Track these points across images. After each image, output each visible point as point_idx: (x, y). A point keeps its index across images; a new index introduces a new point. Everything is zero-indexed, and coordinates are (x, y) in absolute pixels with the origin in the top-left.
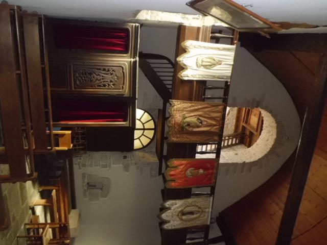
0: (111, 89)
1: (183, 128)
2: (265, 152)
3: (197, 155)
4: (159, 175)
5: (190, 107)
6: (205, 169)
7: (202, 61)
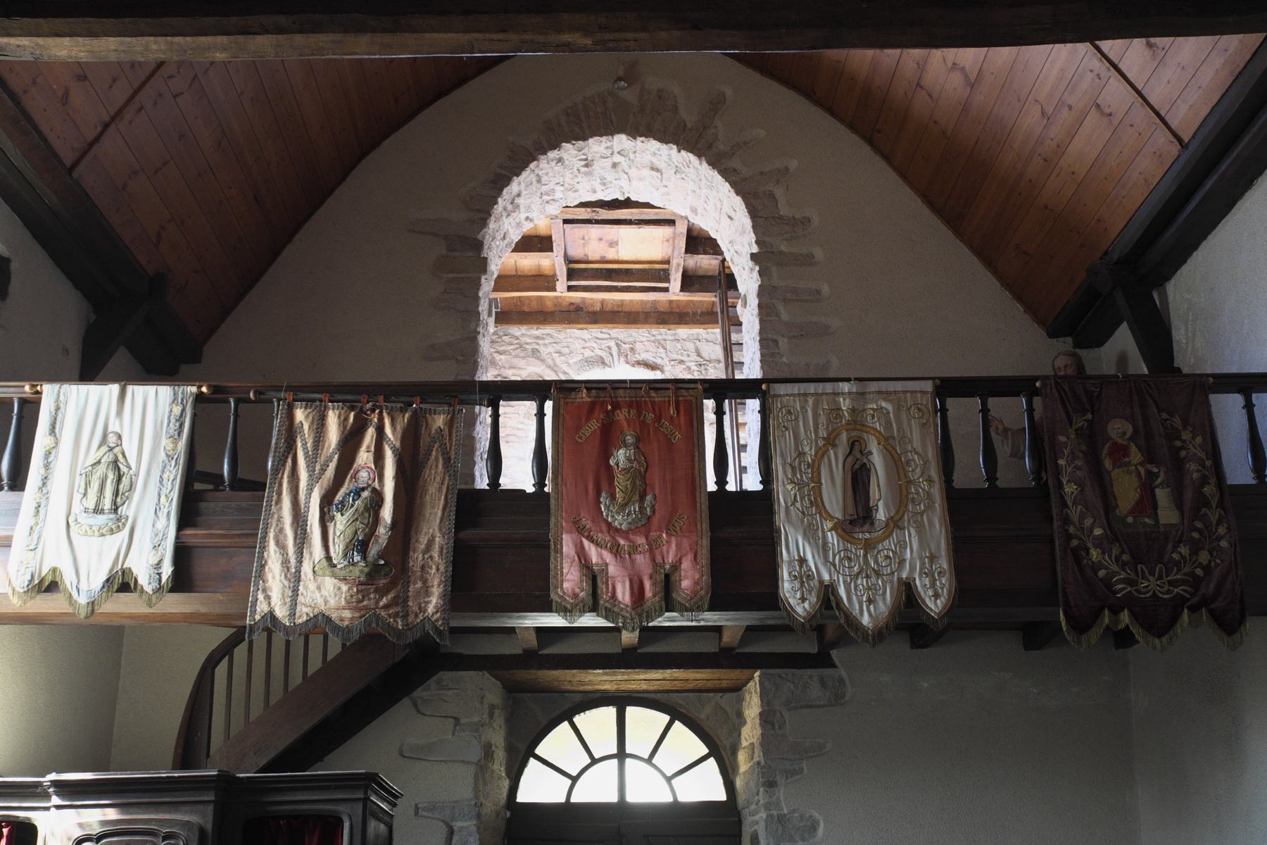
1: (374, 572)
3: (506, 482)
4: (832, 665)
5: (281, 546)
6: (608, 440)
7: (98, 510)
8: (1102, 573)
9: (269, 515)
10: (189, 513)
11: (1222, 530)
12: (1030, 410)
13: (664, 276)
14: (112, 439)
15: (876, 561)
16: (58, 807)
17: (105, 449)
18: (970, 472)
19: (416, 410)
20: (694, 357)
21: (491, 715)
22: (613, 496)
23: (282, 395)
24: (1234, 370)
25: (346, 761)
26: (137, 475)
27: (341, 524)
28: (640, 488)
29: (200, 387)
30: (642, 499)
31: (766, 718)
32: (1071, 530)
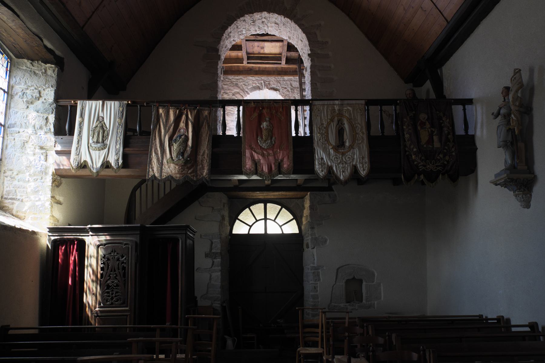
0: (128, 259)
1: (186, 162)
2: (293, 24)
3: (228, 133)
5: (156, 154)
6: (260, 119)
7: (98, 142)
8: (415, 163)
9: (152, 144)
10: (126, 143)
11: (453, 150)
12: (396, 110)
13: (280, 59)
14: (101, 119)
15: (345, 159)
16: (92, 235)
17: (98, 122)
18: (376, 130)
19: (198, 110)
20: (290, 86)
21: (224, 206)
22: (262, 138)
23: (155, 104)
24: (461, 97)
25: (179, 221)
26: (109, 130)
27: (175, 146)
28: (271, 135)
29: (128, 101)
30: (271, 139)
31: (311, 207)
32: (407, 149)
